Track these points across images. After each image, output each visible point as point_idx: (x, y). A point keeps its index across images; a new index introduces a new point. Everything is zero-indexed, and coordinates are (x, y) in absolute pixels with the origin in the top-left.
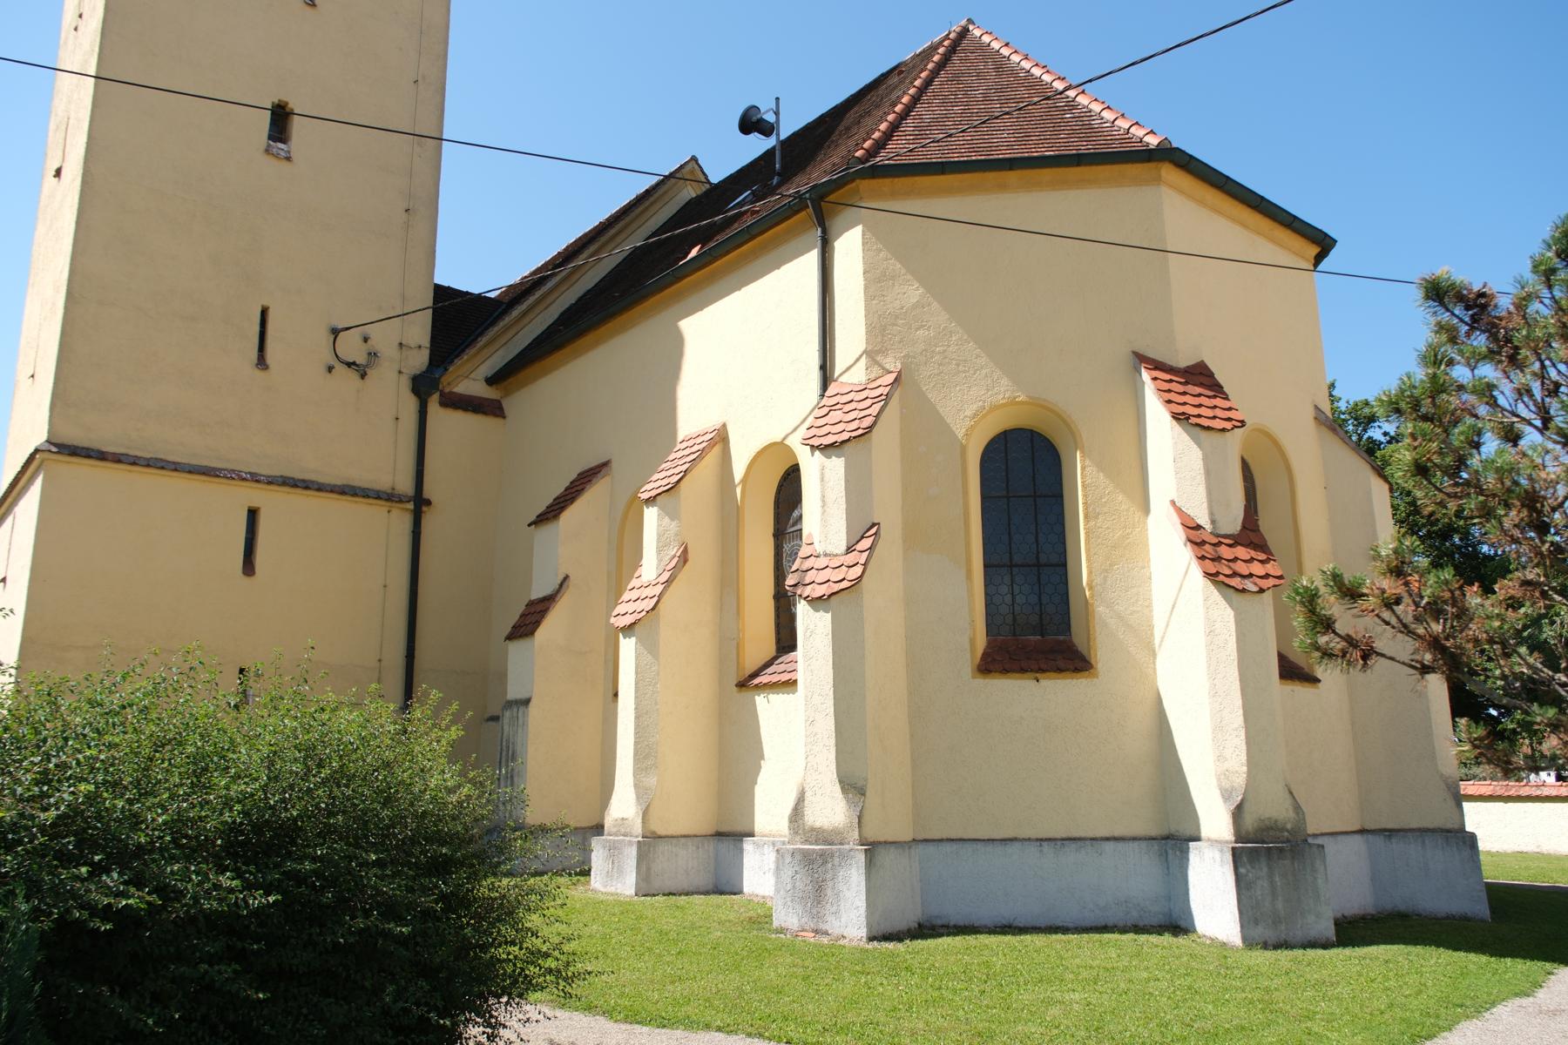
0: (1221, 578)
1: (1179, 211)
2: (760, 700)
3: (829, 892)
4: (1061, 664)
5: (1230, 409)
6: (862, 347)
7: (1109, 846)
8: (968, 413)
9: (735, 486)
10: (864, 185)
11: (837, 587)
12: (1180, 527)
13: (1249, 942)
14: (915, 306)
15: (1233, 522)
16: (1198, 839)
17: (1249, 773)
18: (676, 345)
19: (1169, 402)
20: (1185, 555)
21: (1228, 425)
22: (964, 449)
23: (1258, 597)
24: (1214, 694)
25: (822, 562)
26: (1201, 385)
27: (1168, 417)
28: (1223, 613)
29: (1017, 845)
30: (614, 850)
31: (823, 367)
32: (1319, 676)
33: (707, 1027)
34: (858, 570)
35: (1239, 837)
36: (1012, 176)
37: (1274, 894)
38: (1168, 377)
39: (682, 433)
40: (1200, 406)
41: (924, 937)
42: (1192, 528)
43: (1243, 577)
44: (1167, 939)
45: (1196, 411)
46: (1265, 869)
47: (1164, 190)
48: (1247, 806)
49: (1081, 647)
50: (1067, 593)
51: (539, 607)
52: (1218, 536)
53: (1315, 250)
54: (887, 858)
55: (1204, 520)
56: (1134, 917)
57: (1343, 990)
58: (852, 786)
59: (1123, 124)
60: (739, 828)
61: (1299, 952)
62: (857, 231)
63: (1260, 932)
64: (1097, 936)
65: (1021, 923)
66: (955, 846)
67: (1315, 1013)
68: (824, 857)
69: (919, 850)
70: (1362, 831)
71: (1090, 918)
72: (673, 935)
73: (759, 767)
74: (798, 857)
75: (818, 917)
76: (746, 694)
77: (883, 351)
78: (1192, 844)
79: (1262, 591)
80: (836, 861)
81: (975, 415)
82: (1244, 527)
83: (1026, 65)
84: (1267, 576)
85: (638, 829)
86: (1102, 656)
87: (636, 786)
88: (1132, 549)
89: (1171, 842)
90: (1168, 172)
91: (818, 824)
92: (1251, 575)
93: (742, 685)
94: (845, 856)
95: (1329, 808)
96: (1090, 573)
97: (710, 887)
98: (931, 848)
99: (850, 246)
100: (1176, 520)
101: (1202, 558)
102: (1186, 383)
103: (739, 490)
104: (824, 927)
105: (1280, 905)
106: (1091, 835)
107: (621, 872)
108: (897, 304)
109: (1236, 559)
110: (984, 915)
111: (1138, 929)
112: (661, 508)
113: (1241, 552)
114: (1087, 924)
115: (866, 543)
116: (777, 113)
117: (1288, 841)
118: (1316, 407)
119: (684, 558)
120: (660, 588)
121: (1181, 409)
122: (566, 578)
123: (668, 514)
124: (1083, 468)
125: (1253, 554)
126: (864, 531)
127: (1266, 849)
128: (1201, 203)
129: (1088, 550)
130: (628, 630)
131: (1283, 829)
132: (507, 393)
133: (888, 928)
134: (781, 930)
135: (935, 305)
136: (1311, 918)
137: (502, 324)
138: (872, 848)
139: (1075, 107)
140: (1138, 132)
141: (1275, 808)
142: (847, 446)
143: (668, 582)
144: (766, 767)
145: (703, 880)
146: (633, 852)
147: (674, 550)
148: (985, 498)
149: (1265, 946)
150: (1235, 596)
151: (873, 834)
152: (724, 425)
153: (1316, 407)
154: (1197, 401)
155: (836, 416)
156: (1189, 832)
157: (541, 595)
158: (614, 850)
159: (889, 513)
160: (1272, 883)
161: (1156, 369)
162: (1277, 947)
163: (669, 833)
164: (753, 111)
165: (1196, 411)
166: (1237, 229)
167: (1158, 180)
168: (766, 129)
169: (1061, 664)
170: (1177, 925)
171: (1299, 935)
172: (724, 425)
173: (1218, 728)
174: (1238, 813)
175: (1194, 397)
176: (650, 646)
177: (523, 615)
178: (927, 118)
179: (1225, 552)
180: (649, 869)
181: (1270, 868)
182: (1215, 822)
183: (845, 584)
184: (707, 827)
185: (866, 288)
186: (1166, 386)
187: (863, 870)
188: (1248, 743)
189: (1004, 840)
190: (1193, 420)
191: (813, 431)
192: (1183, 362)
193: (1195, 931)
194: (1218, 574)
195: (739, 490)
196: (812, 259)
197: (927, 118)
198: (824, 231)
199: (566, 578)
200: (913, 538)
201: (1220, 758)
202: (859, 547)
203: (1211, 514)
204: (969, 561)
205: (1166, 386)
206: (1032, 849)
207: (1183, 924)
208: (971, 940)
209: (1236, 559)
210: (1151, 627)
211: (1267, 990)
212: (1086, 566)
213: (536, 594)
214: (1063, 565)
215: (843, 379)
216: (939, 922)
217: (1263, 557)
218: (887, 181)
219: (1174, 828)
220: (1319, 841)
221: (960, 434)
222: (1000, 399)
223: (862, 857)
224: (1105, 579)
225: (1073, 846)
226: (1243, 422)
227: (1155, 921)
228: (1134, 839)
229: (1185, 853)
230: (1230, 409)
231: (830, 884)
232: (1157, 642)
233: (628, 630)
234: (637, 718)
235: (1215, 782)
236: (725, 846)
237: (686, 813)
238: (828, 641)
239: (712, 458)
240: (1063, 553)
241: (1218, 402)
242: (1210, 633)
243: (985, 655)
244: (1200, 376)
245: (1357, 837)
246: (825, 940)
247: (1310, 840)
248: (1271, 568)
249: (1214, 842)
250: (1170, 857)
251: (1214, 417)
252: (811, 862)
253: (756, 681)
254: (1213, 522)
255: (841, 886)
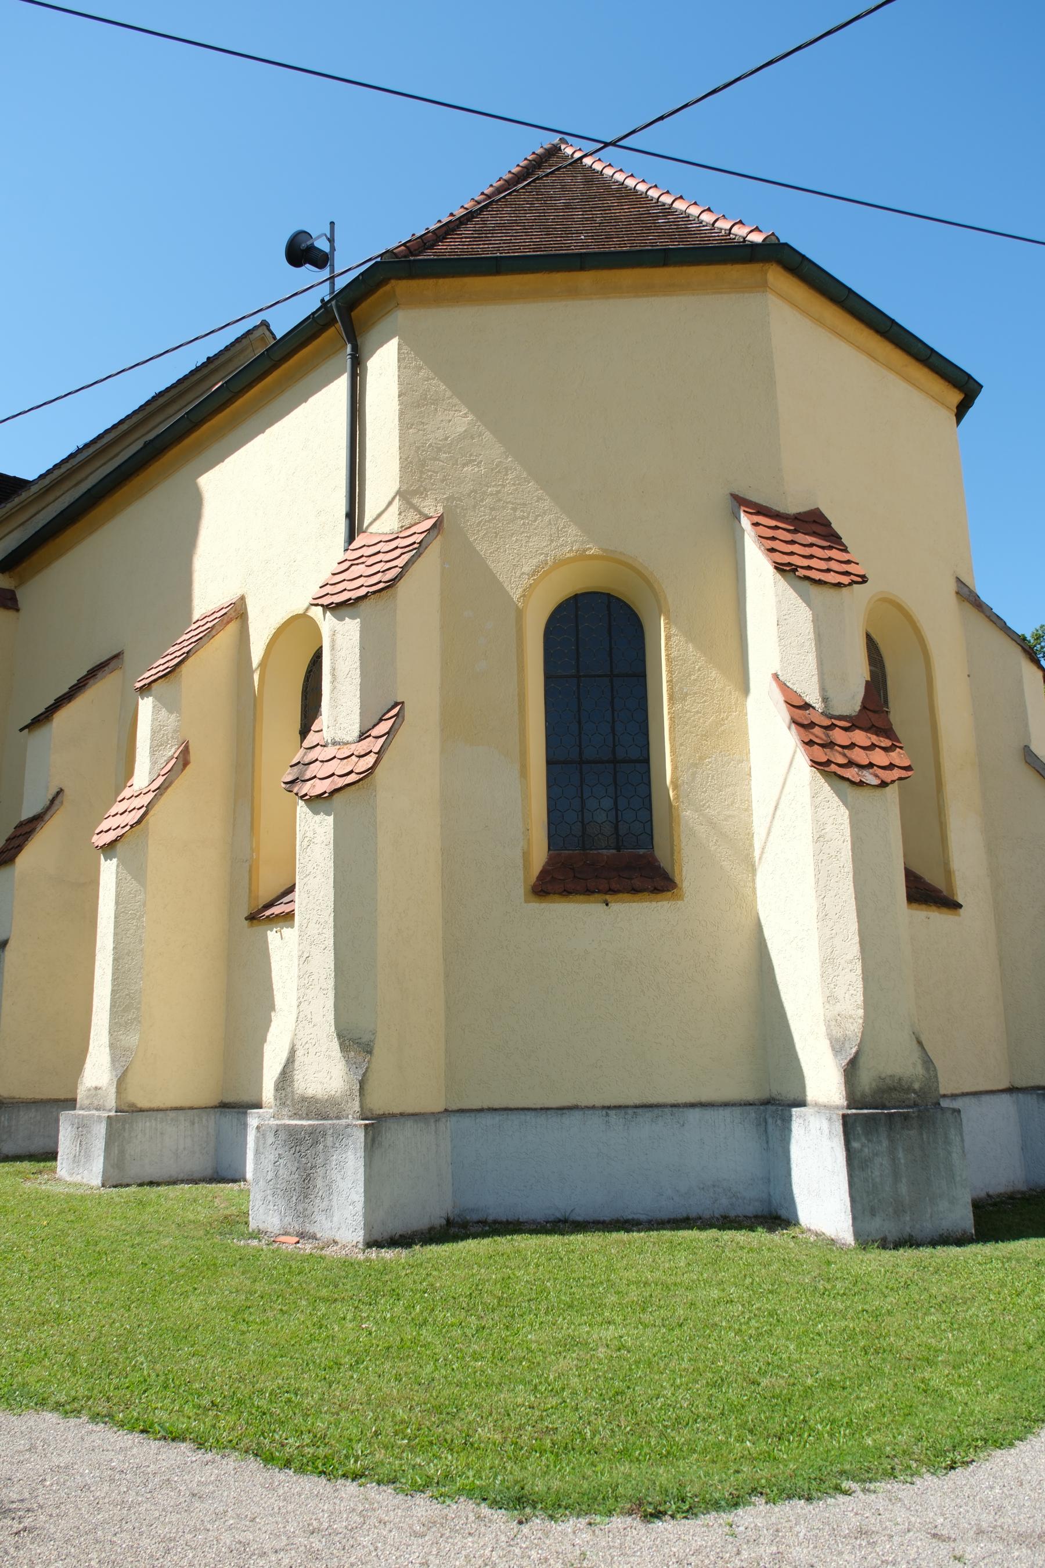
0: (833, 768)
1: (785, 322)
2: (273, 936)
3: (319, 1183)
4: (637, 883)
5: (848, 562)
6: (395, 486)
7: (694, 1115)
8: (526, 569)
9: (253, 672)
10: (401, 287)
11: (341, 782)
12: (783, 707)
13: (864, 1240)
14: (462, 437)
15: (850, 699)
16: (802, 1104)
17: (866, 1017)
18: (195, 501)
19: (772, 550)
20: (789, 740)
21: (845, 580)
22: (520, 614)
23: (878, 792)
24: (823, 916)
25: (330, 752)
26: (814, 534)
27: (770, 569)
28: (837, 814)
29: (577, 1115)
30: (82, 1127)
31: (350, 516)
32: (960, 901)
33: (42, 1403)
34: (370, 760)
35: (853, 1100)
36: (585, 278)
37: (896, 1176)
38: (773, 523)
39: (196, 615)
40: (811, 557)
41: (456, 1238)
42: (798, 707)
43: (861, 767)
44: (760, 1236)
45: (806, 562)
46: (885, 1143)
47: (772, 301)
48: (862, 1060)
49: (664, 864)
50: (650, 795)
51: (26, 829)
52: (832, 717)
53: (956, 397)
54: (399, 1136)
55: (813, 697)
56: (722, 1205)
57: (978, 1312)
58: (355, 1042)
59: (724, 225)
60: (245, 1098)
61: (925, 1252)
62: (393, 344)
63: (877, 1225)
64: (667, 1234)
65: (579, 1216)
66: (497, 1118)
67: (938, 1351)
68: (315, 1136)
69: (450, 1124)
70: (1011, 1090)
71: (668, 1209)
72: (102, 1246)
73: (268, 1022)
74: (283, 1136)
75: (304, 1215)
76: (258, 929)
77: (422, 493)
78: (795, 1111)
79: (884, 784)
80: (329, 1140)
81: (534, 572)
82: (864, 707)
83: (619, 177)
84: (891, 767)
85: (111, 1101)
86: (689, 873)
87: (112, 1046)
88: (727, 738)
89: (770, 1108)
90: (776, 276)
91: (310, 1092)
92: (871, 765)
93: (253, 918)
94: (340, 1134)
95: (968, 1064)
96: (675, 768)
97: (209, 1172)
98: (467, 1121)
99: (384, 364)
100: (779, 698)
101: (810, 743)
102: (795, 531)
103: (256, 677)
104: (311, 1229)
105: (903, 1189)
106: (671, 1100)
107: (88, 1156)
108: (440, 434)
109: (853, 745)
110: (535, 1208)
111: (727, 1222)
112: (157, 698)
113: (860, 737)
114: (664, 1215)
115: (384, 727)
116: (331, 240)
117: (915, 1105)
118: (958, 580)
119: (184, 759)
120: (151, 795)
121: (786, 559)
122: (60, 792)
123: (165, 705)
124: (668, 638)
125: (875, 739)
126: (385, 713)
127: (888, 1116)
128: (819, 321)
129: (673, 740)
130: (109, 849)
131: (909, 1090)
132: (22, 581)
133: (397, 1227)
134: (257, 1235)
135: (488, 436)
136: (943, 1205)
137: (17, 500)
138: (377, 1125)
139: (672, 213)
140: (740, 231)
141: (900, 1063)
142: (364, 605)
143: (161, 790)
144: (273, 1024)
145: (199, 1164)
146: (100, 1130)
147: (172, 751)
148: (549, 677)
149: (884, 1245)
150: (850, 791)
151: (380, 1103)
152: (242, 598)
153: (958, 580)
154: (808, 551)
155: (356, 571)
156: (791, 1096)
157: (31, 815)
158: (82, 1127)
159: (421, 691)
160: (894, 1160)
161: (758, 513)
162: (897, 1245)
163: (155, 1105)
164: (302, 237)
165: (806, 562)
166: (863, 358)
167: (763, 286)
168: (321, 260)
169: (637, 883)
170: (777, 1216)
171: (928, 1227)
172: (242, 598)
173: (828, 961)
174: (851, 1070)
175: (804, 549)
176: (135, 871)
177: (9, 840)
178: (491, 224)
179: (840, 737)
180: (122, 1152)
181: (892, 1141)
182: (824, 1082)
183: (353, 778)
184: (206, 1096)
185: (402, 414)
186: (770, 533)
187: (361, 1153)
188: (865, 979)
189: (562, 1110)
190: (801, 572)
191: (328, 589)
192: (794, 506)
193: (797, 1223)
194: (829, 762)
195: (256, 677)
196: (341, 385)
197: (491, 224)
198: (355, 349)
199: (60, 792)
200: (457, 725)
201: (831, 999)
202: (375, 732)
203: (823, 689)
204: (523, 753)
205: (770, 533)
206: (596, 1120)
207: (783, 1213)
208: (503, 1243)
209: (853, 745)
210: (750, 836)
211: (876, 1315)
212: (670, 762)
213: (26, 814)
214: (647, 761)
215: (373, 529)
216: (475, 1217)
217: (886, 743)
218: (430, 283)
219: (777, 1089)
220: (956, 1104)
221: (516, 594)
222: (567, 552)
223: (360, 1135)
224: (694, 774)
225: (649, 1115)
226: (864, 579)
227: (750, 1210)
228: (726, 1105)
229: (787, 1121)
230: (848, 562)
231: (321, 1171)
232: (757, 859)
233: (109, 849)
234: (115, 960)
235: (822, 1029)
236: (228, 1120)
237: (178, 1077)
238: (329, 852)
239: (226, 637)
240: (646, 746)
241: (834, 553)
242: (819, 838)
243: (544, 873)
244: (814, 525)
245: (1005, 1097)
246: (308, 1247)
247: (945, 1103)
248: (897, 757)
249: (824, 1108)
250: (770, 1128)
251: (828, 570)
252: (299, 1142)
253: (268, 913)
254: (825, 700)
255: (335, 1175)
